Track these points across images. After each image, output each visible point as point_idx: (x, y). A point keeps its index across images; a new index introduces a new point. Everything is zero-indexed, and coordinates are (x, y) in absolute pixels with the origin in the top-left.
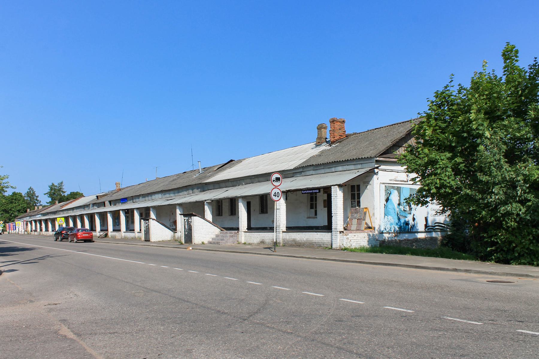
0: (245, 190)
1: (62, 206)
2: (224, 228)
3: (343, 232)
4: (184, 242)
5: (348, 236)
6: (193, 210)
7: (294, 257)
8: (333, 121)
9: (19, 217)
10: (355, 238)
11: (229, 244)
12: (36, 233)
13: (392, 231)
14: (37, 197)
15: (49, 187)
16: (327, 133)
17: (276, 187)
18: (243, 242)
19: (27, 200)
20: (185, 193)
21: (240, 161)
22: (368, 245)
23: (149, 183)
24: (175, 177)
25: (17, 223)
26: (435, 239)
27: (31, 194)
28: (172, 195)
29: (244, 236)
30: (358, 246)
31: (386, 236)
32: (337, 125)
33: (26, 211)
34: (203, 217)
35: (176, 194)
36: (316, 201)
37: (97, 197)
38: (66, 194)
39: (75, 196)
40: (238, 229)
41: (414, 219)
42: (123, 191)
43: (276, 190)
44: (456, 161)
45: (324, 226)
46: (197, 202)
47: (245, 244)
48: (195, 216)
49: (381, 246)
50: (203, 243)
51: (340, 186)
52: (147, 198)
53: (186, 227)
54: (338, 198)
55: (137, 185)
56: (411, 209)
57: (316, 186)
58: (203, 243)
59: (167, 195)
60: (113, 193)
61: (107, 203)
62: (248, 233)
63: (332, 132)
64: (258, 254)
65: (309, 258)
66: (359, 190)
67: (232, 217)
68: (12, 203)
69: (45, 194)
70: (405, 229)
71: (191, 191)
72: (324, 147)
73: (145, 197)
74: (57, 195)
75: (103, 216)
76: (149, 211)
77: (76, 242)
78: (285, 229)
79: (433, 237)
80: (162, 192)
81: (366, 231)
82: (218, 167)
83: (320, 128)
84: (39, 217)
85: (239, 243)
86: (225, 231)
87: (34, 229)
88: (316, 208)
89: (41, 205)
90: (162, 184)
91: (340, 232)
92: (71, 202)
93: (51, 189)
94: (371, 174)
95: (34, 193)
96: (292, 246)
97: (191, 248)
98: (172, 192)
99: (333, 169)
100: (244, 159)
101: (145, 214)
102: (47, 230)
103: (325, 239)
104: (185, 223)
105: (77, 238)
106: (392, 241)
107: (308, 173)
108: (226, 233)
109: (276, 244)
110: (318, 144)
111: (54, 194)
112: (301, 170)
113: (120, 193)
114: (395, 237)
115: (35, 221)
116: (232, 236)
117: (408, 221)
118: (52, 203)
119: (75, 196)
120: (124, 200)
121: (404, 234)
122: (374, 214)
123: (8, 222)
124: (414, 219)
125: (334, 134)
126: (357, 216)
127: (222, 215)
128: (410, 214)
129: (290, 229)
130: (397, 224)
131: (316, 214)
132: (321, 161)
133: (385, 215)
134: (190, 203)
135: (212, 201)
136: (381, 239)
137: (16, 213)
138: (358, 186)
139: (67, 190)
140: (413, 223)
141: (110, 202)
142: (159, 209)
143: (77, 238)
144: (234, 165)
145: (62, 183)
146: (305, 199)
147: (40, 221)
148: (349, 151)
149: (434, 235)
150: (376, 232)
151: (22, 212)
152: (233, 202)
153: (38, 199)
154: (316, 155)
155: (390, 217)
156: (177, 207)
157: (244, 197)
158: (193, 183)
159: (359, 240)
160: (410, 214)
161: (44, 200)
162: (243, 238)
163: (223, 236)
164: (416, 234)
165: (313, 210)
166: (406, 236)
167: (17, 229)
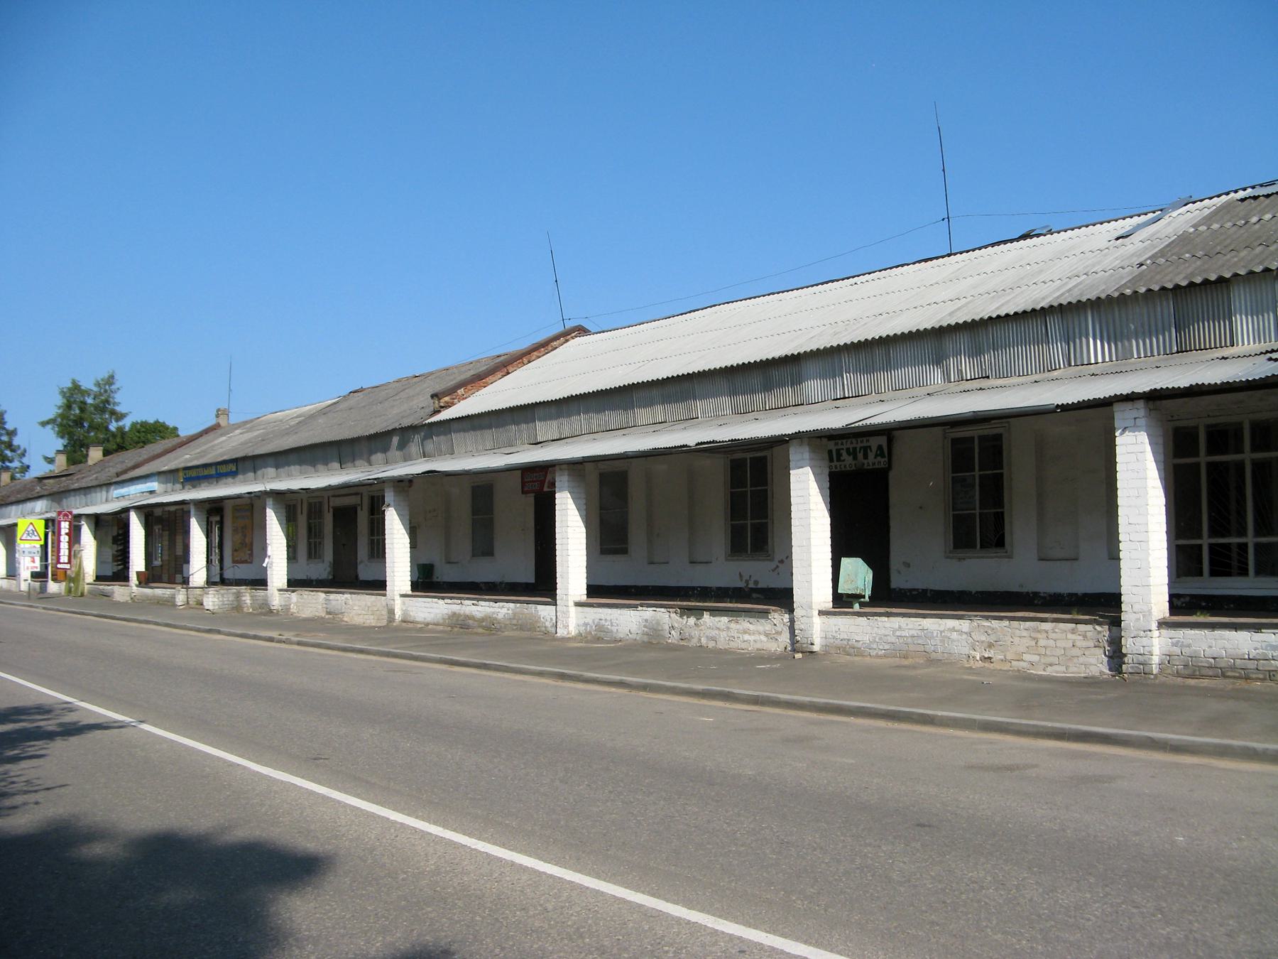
14: (12, 433)
15: (63, 393)
20: (1032, 353)
38: (127, 423)
45: (527, 584)
65: (756, 701)
69: (44, 424)
145: (110, 380)
152: (251, 508)
153: (16, 441)
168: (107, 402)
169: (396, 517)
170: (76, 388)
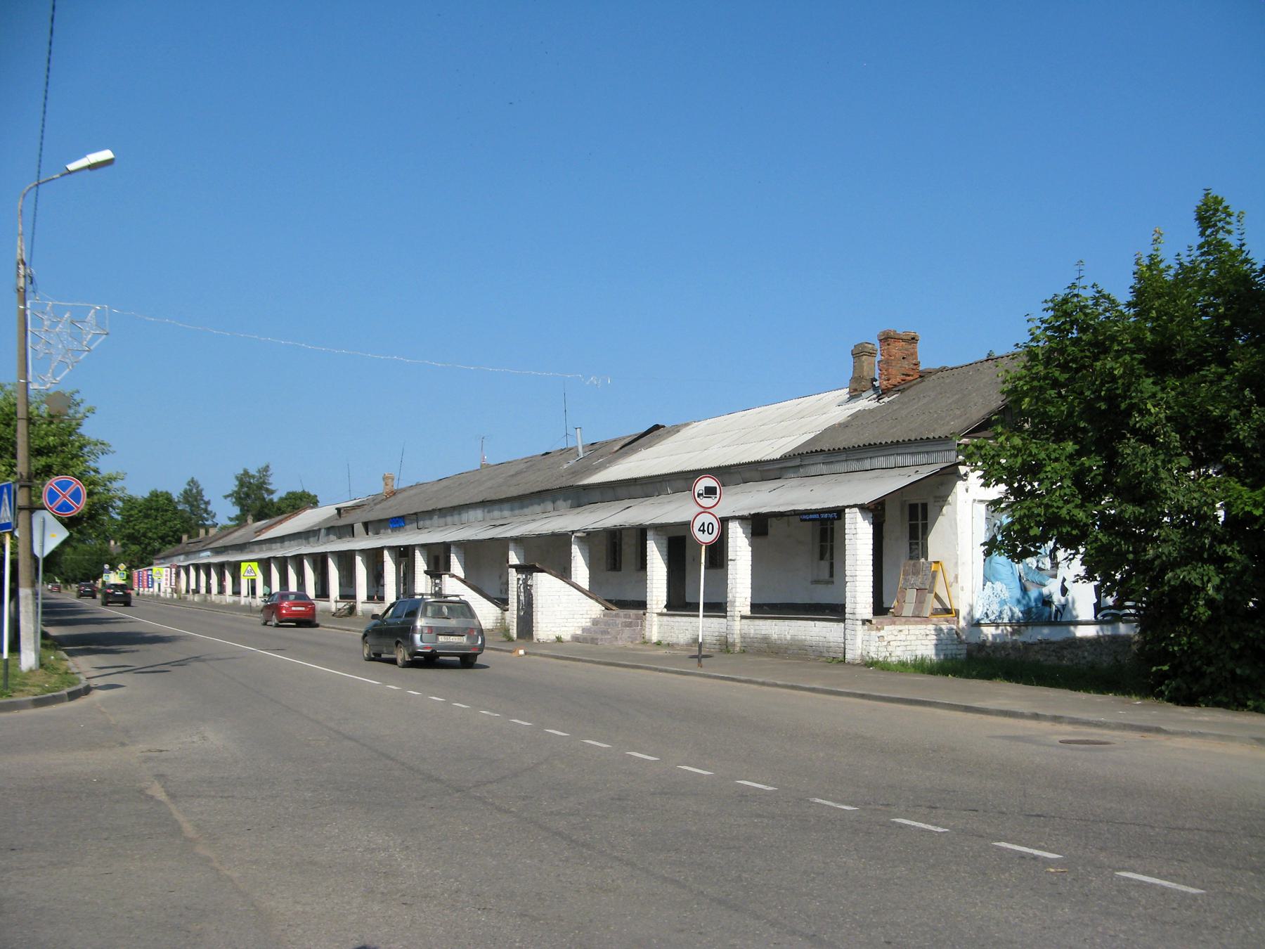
0: (668, 508)
1: (260, 531)
2: (610, 601)
3: (870, 621)
4: (515, 636)
5: (882, 633)
6: (549, 555)
7: (733, 680)
8: (886, 339)
9: (162, 554)
10: (902, 636)
11: (620, 643)
12: (196, 598)
13: (1006, 620)
14: (208, 503)
16: (872, 367)
17: (705, 510)
18: (655, 639)
19: (183, 511)
20: (537, 508)
21: (676, 429)
22: (937, 654)
23: (462, 479)
24: (522, 466)
25: (155, 569)
26: (1126, 640)
27: (194, 496)
28: (506, 513)
29: (659, 625)
30: (908, 657)
31: (989, 632)
32: (897, 349)
33: (179, 541)
34: (564, 573)
35: (517, 512)
36: (832, 541)
37: (339, 510)
38: (275, 498)
39: (299, 502)
40: (642, 605)
41: (1064, 591)
42: (400, 496)
43: (707, 519)
44: (1083, 464)
46: (554, 535)
47: (659, 644)
48: (542, 571)
49: (970, 659)
50: (559, 639)
51: (862, 508)
52: (449, 519)
53: (522, 598)
54: (859, 536)
55: (433, 483)
56: (1055, 565)
57: (814, 507)
58: (559, 639)
59: (496, 514)
60: (376, 500)
61: (359, 528)
62: (665, 618)
63: (886, 364)
64: (661, 671)
65: (763, 684)
66: (925, 517)
67: (613, 573)
68: (147, 516)
69: (226, 497)
70: (1040, 615)
71: (549, 506)
72: (866, 403)
73: (445, 516)
74: (256, 501)
75: (346, 561)
76: (449, 552)
77: (277, 626)
78: (747, 611)
79: (1123, 637)
80: (485, 504)
81: (935, 619)
82: (623, 443)
83: (859, 353)
84: (206, 557)
85: (645, 643)
86: (616, 611)
87: (193, 586)
88: (832, 558)
89: (215, 525)
90: (489, 484)
91: (864, 622)
92: (280, 522)
93: (242, 484)
94: (951, 477)
95: (200, 493)
96: (759, 652)
97: (522, 652)
98: (506, 506)
99: (867, 464)
100: (687, 425)
101: (438, 562)
102: (222, 591)
103: (831, 639)
104: (519, 588)
105: (279, 615)
106: (1003, 645)
107: (813, 470)
108: (617, 616)
109: (725, 646)
110: (854, 395)
111: (248, 495)
112: (797, 462)
113: (392, 501)
114: (1012, 634)
115: (197, 567)
116: (629, 625)
117: (1050, 596)
118: (240, 521)
119: (299, 502)
120: (397, 522)
121: (1037, 629)
122: (956, 577)
123: (137, 567)
124: (1064, 591)
125: (889, 369)
126: (917, 581)
127: (620, 570)
128: (1055, 576)
129: (760, 609)
130: (1019, 602)
131: (832, 575)
132: (841, 442)
133: (986, 579)
134: (539, 536)
135: (589, 534)
136: (973, 640)
137: (157, 545)
138: (925, 506)
139: (280, 488)
140: (1063, 600)
141: (366, 525)
142: (470, 550)
143: (279, 615)
144: (661, 438)
145: (267, 469)
146: (807, 532)
147: (207, 567)
148: (918, 414)
149: (1123, 629)
150: (962, 623)
151: (170, 542)
153: (210, 508)
154: (840, 424)
155: (998, 585)
156: (511, 545)
157: (660, 528)
158: (556, 485)
159: (913, 640)
160: (1055, 576)
161: (224, 511)
162: (655, 629)
163: (606, 624)
164: (1072, 628)
165: (825, 565)
166: (1045, 633)
167: (156, 585)
168: (264, 483)
169: (655, 549)
170: (246, 473)
